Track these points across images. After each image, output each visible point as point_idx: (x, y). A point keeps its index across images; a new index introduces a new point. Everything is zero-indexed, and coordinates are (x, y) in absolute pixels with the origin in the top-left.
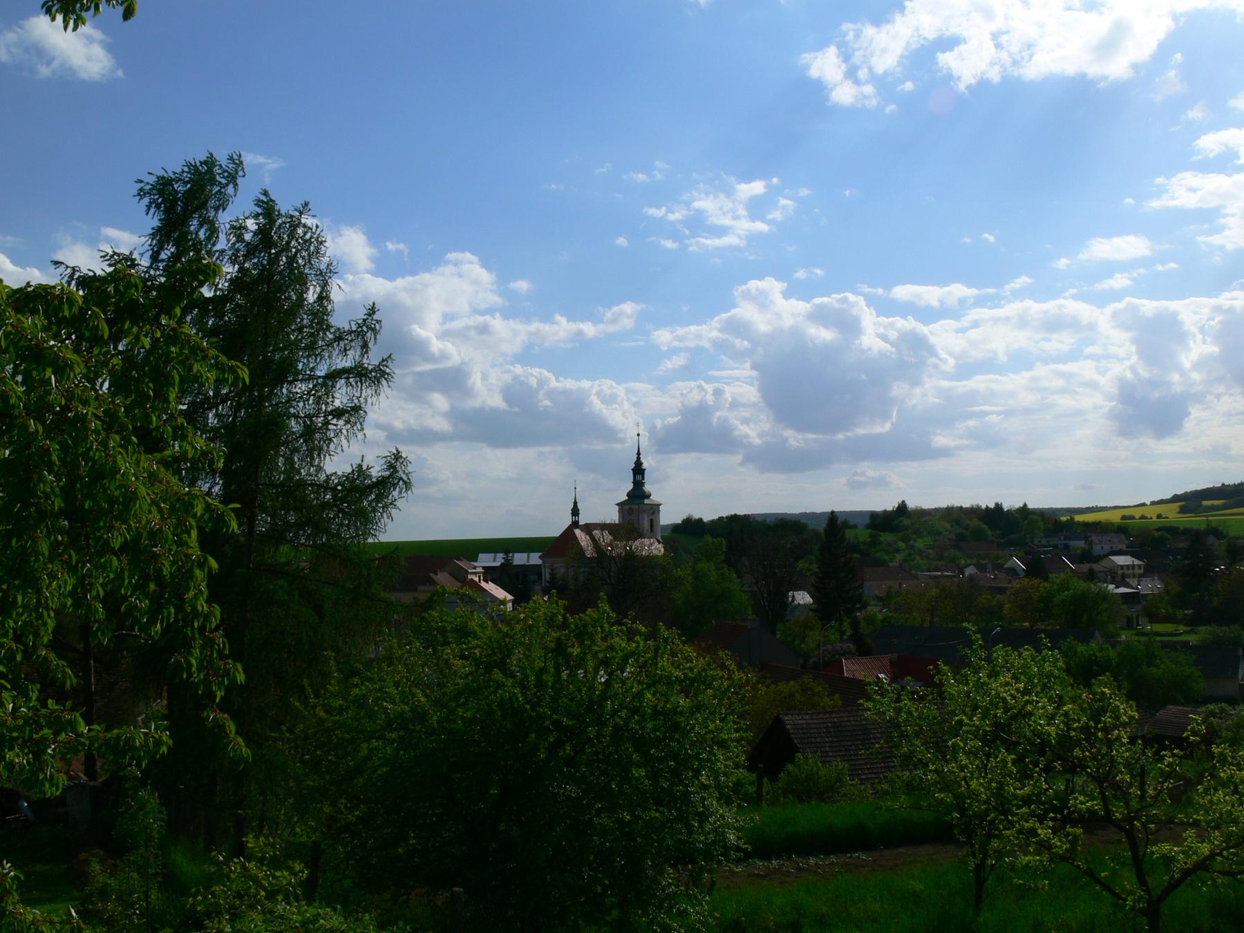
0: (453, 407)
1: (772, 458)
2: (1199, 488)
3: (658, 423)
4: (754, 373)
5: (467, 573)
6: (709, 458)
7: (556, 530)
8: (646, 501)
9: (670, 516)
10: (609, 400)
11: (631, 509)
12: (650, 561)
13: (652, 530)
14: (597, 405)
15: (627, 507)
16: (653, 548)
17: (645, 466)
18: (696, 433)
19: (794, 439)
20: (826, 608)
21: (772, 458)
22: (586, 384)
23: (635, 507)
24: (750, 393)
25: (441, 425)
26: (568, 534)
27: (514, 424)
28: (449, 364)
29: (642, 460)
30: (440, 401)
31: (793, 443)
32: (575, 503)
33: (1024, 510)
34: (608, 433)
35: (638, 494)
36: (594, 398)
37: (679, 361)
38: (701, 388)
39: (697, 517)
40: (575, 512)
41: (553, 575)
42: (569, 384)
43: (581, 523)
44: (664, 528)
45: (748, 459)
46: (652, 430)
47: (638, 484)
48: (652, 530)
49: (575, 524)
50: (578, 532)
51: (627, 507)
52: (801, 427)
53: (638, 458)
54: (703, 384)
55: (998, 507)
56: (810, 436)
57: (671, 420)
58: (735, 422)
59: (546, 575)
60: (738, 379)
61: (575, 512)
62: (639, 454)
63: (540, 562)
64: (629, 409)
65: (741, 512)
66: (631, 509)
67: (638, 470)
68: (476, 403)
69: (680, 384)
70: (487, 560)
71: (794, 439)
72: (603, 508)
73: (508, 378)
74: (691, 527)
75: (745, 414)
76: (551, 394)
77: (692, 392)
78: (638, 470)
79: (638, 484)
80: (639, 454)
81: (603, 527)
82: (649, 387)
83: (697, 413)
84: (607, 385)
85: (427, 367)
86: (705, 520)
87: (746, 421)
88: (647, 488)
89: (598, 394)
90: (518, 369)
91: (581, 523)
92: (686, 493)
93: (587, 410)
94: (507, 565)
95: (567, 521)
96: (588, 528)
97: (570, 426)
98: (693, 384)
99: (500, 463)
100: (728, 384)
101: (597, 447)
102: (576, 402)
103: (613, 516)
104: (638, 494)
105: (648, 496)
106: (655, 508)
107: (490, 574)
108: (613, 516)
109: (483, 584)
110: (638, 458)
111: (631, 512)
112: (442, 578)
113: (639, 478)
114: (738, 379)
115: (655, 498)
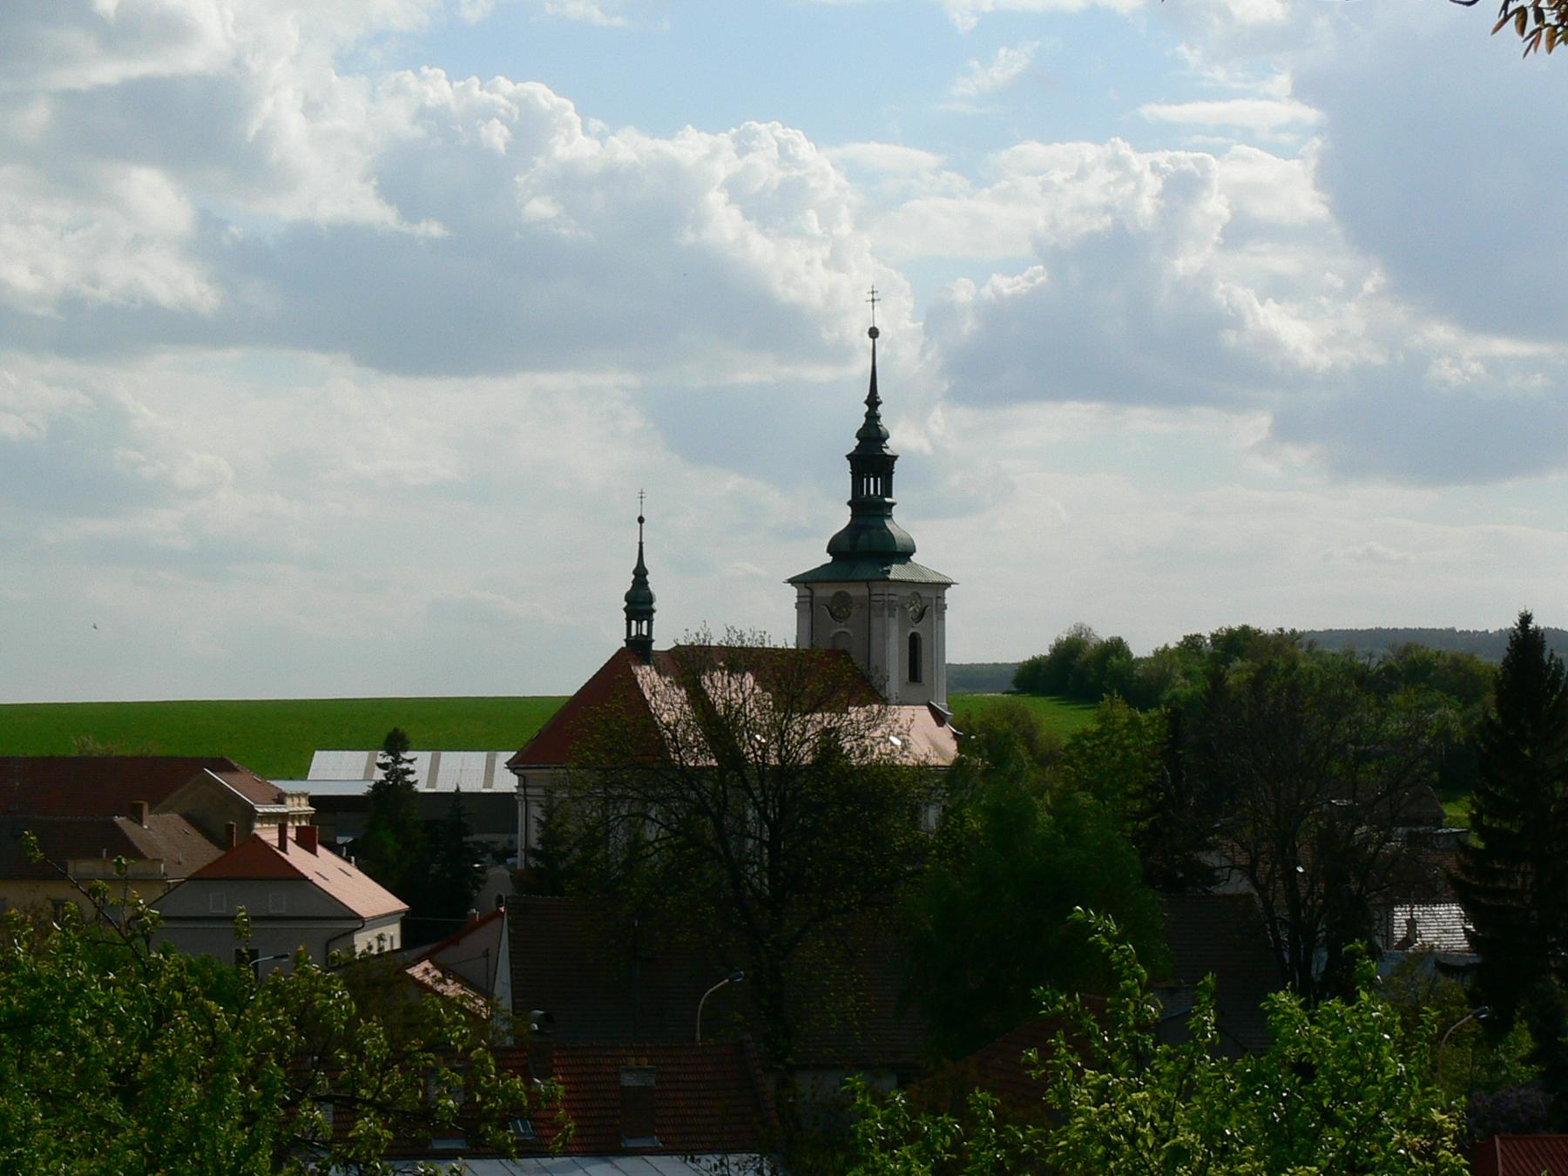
0: (208, 223)
1: (1387, 430)
2: (1384, 627)
3: (963, 292)
4: (1310, 115)
5: (250, 815)
6: (1144, 422)
7: (564, 676)
8: (897, 572)
9: (993, 624)
10: (774, 208)
11: (842, 601)
12: (890, 787)
13: (915, 675)
14: (724, 224)
15: (825, 592)
16: (917, 736)
17: (892, 445)
18: (1103, 335)
19: (1462, 356)
20: (314, 1054)
21: (1387, 430)
22: (689, 146)
23: (856, 591)
24: (1292, 189)
25: (176, 282)
26: (614, 679)
27: (430, 292)
28: (193, 60)
29: (885, 422)
30: (154, 195)
31: (1446, 372)
32: (640, 573)
33: (1156, 652)
34: (777, 326)
35: (867, 545)
36: (716, 199)
37: (1008, 64)
38: (1117, 163)
39: (1236, 626)
40: (639, 604)
41: (551, 836)
42: (628, 147)
43: (662, 641)
44: (971, 677)
45: (1288, 429)
46: (937, 317)
47: (870, 508)
48: (915, 675)
49: (638, 648)
50: (646, 676)
51: (825, 592)
52: (1481, 314)
53: (872, 417)
54: (1125, 149)
55: (1452, 630)
56: (1503, 347)
57: (1005, 285)
58: (1244, 296)
59: (528, 832)
60: (1248, 136)
61: (639, 604)
62: (873, 401)
63: (507, 782)
64: (864, 239)
65: (1267, 624)
66: (842, 601)
67: (871, 460)
68: (286, 210)
69: (1035, 150)
70: (344, 771)
71: (1462, 356)
72: (741, 589)
73: (397, 117)
74: (1080, 670)
75: (1283, 263)
76: (567, 183)
77: (1069, 181)
78: (871, 460)
79: (870, 508)
80: (873, 401)
81: (739, 658)
82: (926, 159)
83: (1114, 253)
84: (780, 147)
85: (108, 72)
86: (1142, 648)
87: (1278, 289)
88: (901, 523)
89: (735, 189)
90: (437, 88)
91: (662, 641)
92: (1049, 552)
93: (689, 237)
94: (392, 795)
95: (613, 637)
96: (690, 663)
97: (616, 292)
98: (1090, 152)
99: (398, 428)
100: (1218, 152)
101: (746, 378)
102: (659, 210)
103: (779, 625)
104: (867, 545)
105: (905, 554)
106: (928, 599)
107: (331, 821)
108: (779, 625)
109: (296, 856)
110: (872, 417)
111: (840, 608)
112: (165, 837)
113: (872, 486)
114: (1248, 136)
115: (929, 560)
